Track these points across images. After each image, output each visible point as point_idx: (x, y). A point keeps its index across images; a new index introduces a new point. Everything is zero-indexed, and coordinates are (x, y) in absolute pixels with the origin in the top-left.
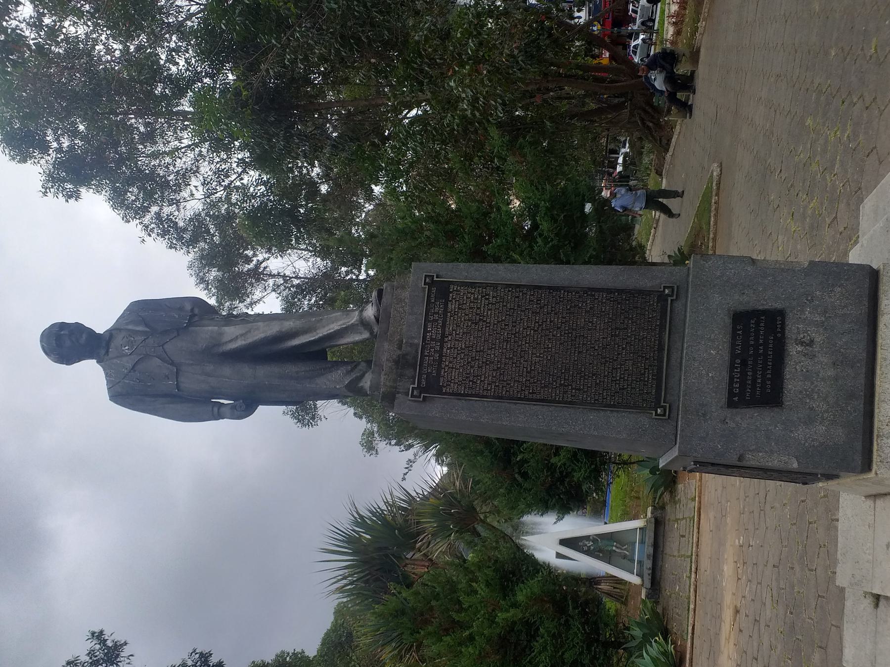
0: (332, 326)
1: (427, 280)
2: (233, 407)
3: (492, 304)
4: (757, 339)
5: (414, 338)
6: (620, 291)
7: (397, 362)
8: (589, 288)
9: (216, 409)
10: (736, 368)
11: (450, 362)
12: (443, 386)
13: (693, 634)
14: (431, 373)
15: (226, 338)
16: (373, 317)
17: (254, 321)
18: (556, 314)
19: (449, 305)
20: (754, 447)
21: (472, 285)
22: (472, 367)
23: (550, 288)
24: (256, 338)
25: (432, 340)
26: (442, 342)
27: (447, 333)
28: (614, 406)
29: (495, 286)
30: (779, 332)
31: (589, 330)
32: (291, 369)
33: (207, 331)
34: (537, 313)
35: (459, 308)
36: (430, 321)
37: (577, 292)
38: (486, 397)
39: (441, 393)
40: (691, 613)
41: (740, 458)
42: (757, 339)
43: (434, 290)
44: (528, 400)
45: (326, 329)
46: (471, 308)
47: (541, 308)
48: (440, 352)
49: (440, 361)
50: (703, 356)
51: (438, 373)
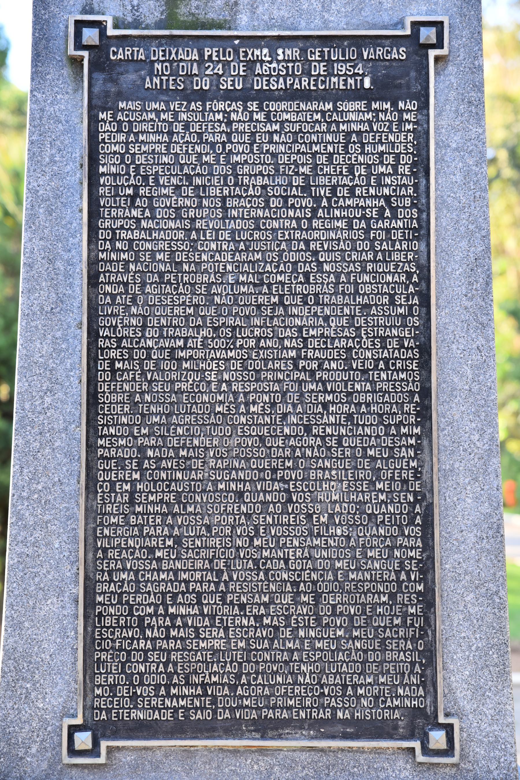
3: (367, 230)
6: (428, 600)
8: (430, 508)
11: (186, 127)
12: (116, 110)
18: (350, 417)
21: (421, 166)
23: (426, 393)
25: (250, 65)
26: (245, 96)
27: (273, 106)
28: (90, 603)
29: (421, 232)
35: (348, 134)
36: (303, 51)
37: (417, 474)
39: (93, 110)
43: (400, 53)
47: (365, 372)
49: (189, 96)
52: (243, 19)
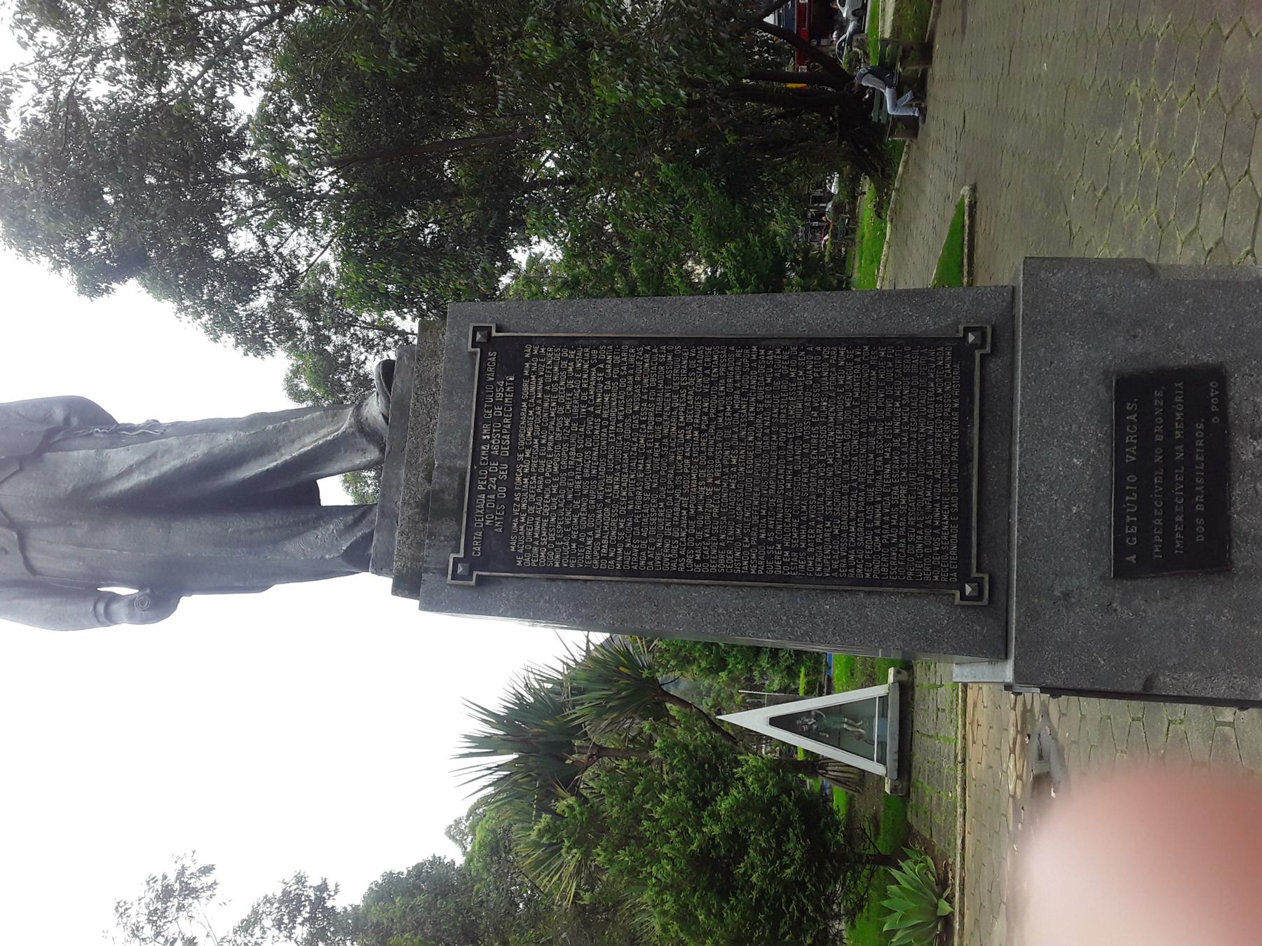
0: (308, 440)
1: (479, 336)
2: (131, 602)
4: (1169, 431)
5: (455, 456)
6: (876, 342)
7: (424, 506)
9: (101, 607)
10: (1130, 493)
11: (530, 504)
13: (963, 848)
14: (492, 527)
15: (112, 470)
16: (380, 418)
17: (163, 435)
18: (743, 395)
19: (525, 386)
20: (1176, 660)
21: (571, 343)
22: (574, 512)
23: (728, 342)
24: (165, 468)
25: (491, 458)
26: (513, 462)
28: (871, 583)
29: (616, 343)
30: (1215, 414)
31: (813, 424)
32: (237, 525)
33: (76, 460)
34: (703, 395)
35: (545, 392)
36: (486, 421)
38: (606, 573)
40: (960, 820)
41: (1149, 682)
42: (1169, 431)
43: (492, 356)
44: (693, 576)
45: (297, 445)
46: (568, 390)
47: (711, 383)
48: (510, 483)
50: (1057, 463)
51: (507, 526)
52: (459, 463)
